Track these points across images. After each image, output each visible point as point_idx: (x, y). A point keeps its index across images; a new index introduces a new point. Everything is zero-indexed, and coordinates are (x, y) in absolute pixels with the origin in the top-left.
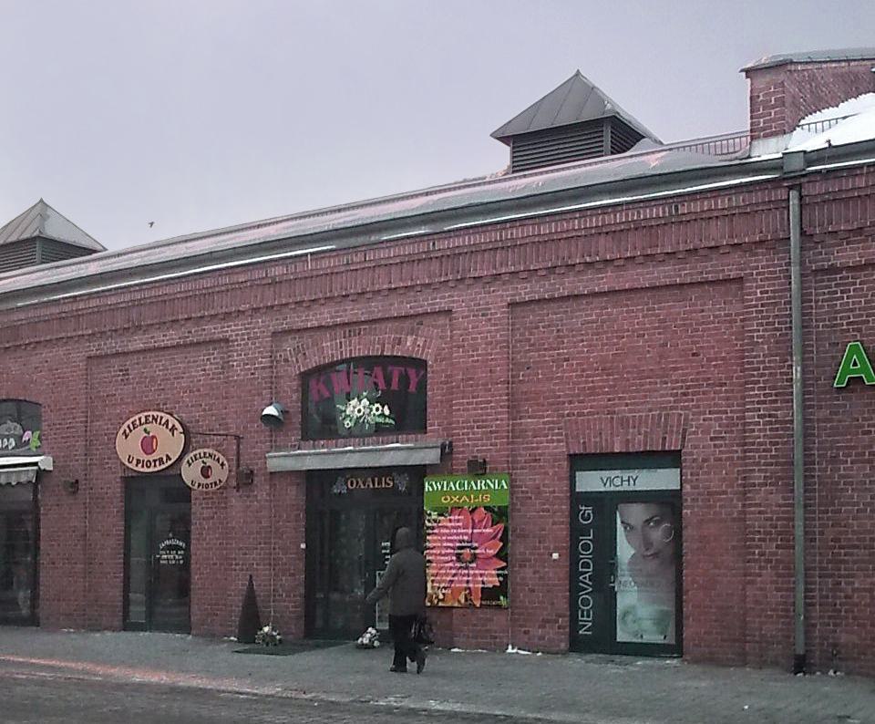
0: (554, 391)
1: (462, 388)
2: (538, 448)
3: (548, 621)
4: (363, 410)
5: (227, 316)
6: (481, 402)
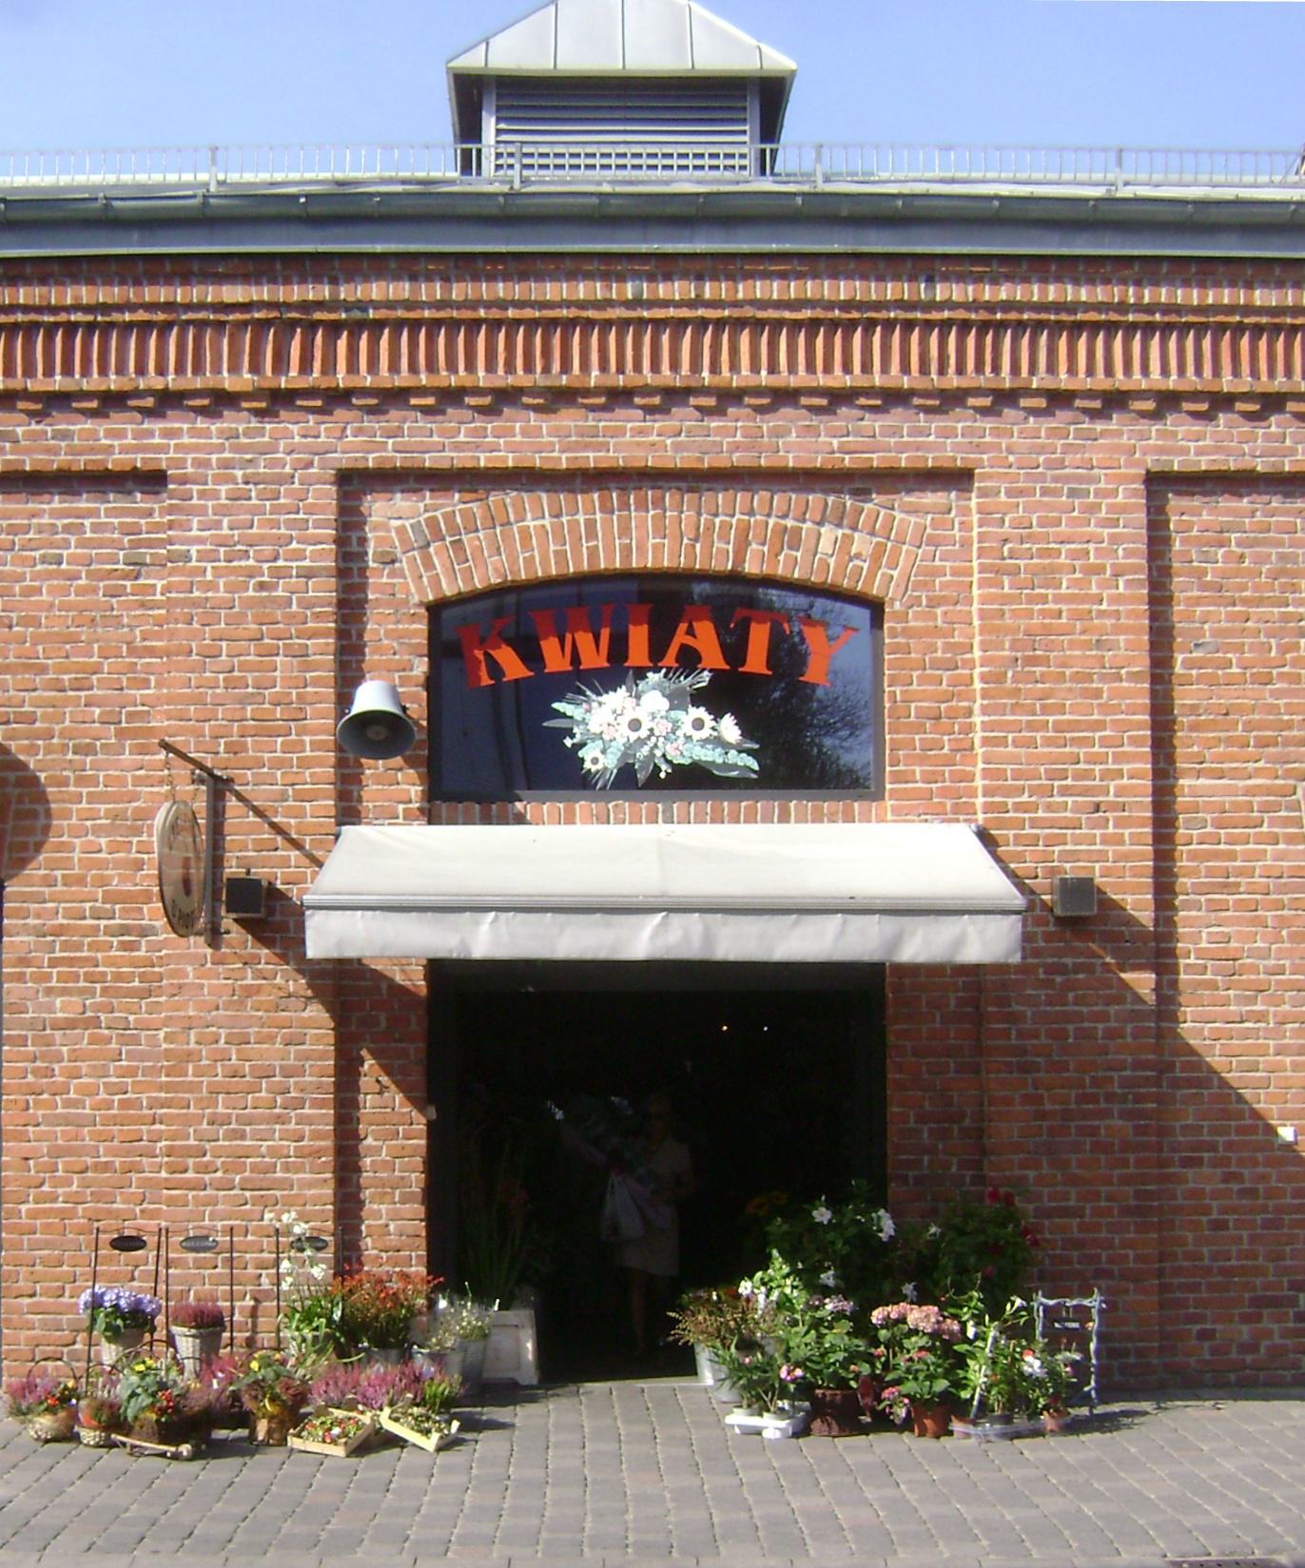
0: (1273, 709)
1: (1009, 684)
2: (1231, 856)
3: (1275, 1302)
4: (646, 725)
5: (168, 401)
6: (1074, 726)
